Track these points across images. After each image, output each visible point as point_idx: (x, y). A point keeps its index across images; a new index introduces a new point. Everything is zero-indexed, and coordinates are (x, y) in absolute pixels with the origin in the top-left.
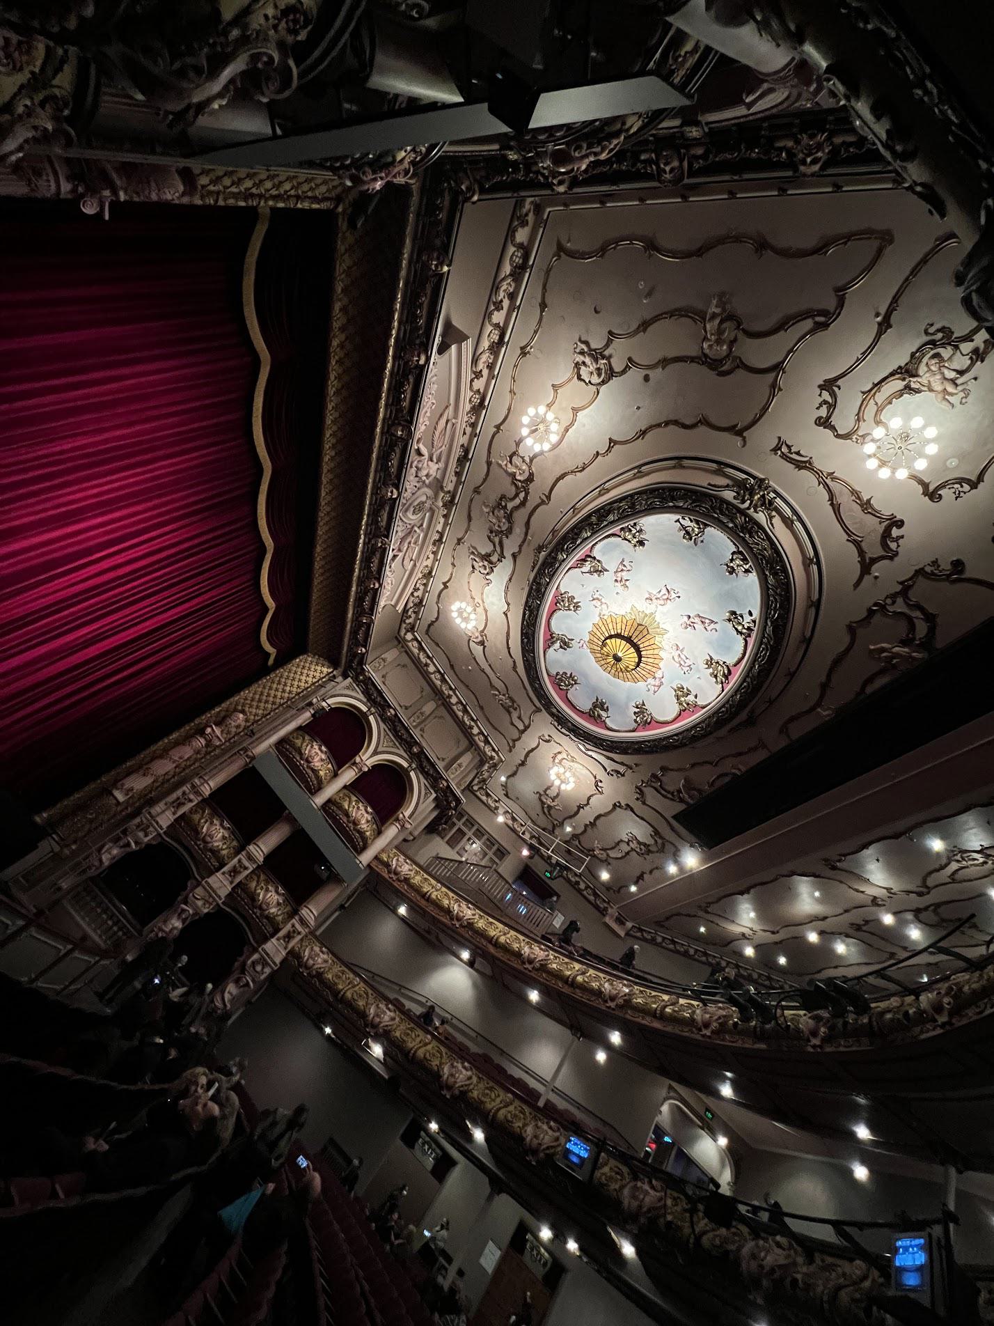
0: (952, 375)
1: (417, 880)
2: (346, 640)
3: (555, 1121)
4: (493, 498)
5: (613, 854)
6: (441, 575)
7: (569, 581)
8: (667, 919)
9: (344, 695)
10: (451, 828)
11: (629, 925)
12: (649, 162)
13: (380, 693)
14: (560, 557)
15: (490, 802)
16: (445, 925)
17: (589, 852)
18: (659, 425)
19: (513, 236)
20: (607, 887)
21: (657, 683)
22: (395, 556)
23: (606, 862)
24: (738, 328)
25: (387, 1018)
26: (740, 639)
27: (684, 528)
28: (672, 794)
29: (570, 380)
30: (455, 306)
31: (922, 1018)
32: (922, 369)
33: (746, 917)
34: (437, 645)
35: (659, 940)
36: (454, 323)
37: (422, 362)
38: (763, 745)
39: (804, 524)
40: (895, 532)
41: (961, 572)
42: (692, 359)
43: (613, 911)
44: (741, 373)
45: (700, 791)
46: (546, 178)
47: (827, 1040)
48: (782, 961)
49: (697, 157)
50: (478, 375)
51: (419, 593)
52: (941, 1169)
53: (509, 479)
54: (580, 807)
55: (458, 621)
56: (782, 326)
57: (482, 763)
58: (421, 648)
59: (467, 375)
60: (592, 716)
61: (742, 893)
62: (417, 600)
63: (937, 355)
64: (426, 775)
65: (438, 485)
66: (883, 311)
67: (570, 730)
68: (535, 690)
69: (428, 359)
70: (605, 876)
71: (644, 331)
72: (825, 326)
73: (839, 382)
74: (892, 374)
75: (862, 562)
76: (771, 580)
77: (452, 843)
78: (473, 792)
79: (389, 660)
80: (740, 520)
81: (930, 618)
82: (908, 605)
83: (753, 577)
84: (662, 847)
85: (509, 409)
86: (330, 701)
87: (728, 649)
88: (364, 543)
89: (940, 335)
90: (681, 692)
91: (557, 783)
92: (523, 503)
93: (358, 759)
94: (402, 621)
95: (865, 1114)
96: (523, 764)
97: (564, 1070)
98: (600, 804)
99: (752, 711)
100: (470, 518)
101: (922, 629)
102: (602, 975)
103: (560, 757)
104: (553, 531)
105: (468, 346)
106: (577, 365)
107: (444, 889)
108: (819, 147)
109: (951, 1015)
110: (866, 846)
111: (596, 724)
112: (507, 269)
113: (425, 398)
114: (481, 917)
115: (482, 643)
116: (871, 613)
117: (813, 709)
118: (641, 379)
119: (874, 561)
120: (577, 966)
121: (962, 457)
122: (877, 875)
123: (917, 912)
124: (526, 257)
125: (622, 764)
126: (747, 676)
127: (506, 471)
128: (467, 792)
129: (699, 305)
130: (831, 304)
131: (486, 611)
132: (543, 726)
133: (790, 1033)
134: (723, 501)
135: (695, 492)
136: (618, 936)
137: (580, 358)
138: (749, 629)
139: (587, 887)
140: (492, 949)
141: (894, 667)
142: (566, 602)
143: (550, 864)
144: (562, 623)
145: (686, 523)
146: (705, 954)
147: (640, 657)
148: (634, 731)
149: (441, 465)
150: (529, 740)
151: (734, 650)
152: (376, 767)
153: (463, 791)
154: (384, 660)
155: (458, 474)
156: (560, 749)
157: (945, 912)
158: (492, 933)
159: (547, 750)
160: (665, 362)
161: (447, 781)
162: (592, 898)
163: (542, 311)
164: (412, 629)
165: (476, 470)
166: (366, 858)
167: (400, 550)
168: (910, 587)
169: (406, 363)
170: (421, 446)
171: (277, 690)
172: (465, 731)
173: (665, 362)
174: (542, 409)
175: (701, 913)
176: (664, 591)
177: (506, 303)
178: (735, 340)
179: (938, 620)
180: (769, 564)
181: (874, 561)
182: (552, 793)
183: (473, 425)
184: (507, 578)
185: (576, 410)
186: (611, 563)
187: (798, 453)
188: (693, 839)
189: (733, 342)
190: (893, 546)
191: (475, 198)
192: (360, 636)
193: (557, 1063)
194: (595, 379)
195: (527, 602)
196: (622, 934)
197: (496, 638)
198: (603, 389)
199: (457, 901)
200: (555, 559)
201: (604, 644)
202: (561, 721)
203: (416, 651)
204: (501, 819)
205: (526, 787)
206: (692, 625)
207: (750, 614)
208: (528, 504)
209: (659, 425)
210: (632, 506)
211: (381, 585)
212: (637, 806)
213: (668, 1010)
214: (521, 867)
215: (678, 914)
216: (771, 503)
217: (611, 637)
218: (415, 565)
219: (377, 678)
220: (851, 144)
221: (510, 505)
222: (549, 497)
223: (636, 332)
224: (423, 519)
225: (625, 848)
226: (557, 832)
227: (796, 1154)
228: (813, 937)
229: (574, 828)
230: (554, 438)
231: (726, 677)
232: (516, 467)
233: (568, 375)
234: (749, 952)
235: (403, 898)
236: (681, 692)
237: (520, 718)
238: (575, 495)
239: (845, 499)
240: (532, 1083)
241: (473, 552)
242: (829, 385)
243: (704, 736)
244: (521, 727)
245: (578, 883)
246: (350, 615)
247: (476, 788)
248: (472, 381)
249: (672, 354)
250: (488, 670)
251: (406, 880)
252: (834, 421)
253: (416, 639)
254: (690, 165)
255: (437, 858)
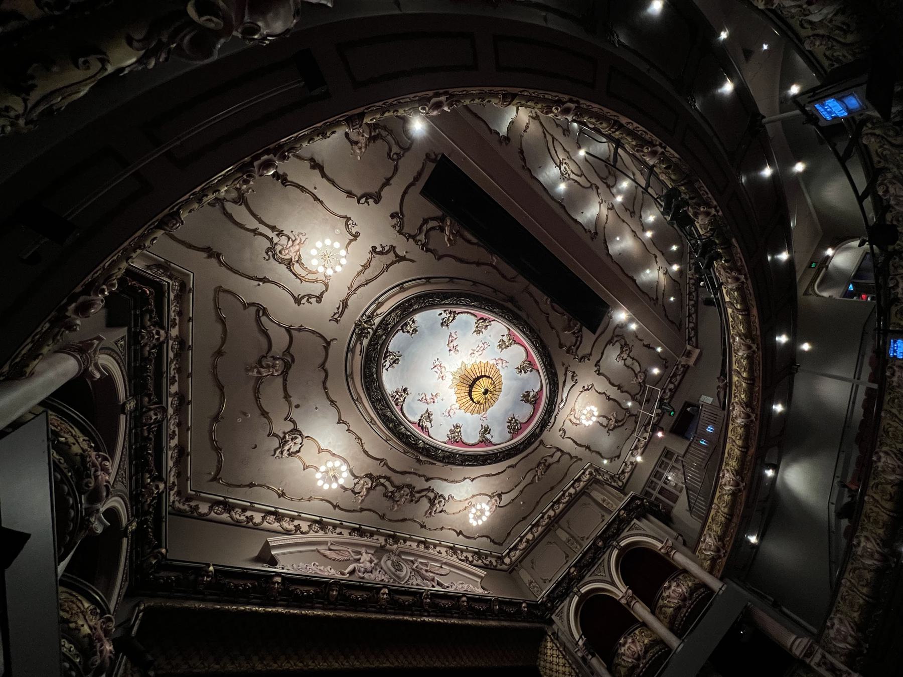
0: (290, 242)
1: (717, 529)
2: (517, 624)
3: (884, 372)
4: (387, 503)
5: (637, 369)
6: (451, 538)
7: (439, 436)
8: (672, 322)
9: (568, 619)
10: (661, 501)
11: (689, 347)
12: (149, 431)
13: (559, 584)
14: (421, 445)
15: (628, 470)
16: (748, 497)
17: (642, 386)
18: (327, 393)
19: (204, 515)
20: (664, 367)
21: (500, 362)
22: (439, 584)
23: (646, 372)
24: (266, 357)
25: (869, 545)
26: (457, 317)
27: (391, 365)
28: (577, 337)
29: (300, 458)
30: (242, 557)
31: (664, 159)
32: (288, 257)
33: (652, 275)
34: (509, 534)
35: (692, 325)
36: (256, 554)
37: (279, 579)
38: (526, 289)
39: (381, 296)
40: (379, 249)
41: (397, 213)
42: (285, 380)
43: (683, 360)
44: (292, 351)
45: (570, 320)
46: (154, 498)
47: (708, 205)
48: (674, 248)
49: (150, 400)
50: (298, 528)
51: (470, 556)
52: (767, 126)
53: (372, 492)
54: (609, 399)
55: (485, 519)
56: (265, 333)
57: (597, 481)
58: (515, 548)
59: (298, 538)
60: (535, 402)
61: (635, 281)
62: (476, 557)
63: (280, 252)
64: (619, 531)
65: (380, 551)
66: (256, 283)
67: (550, 417)
68: (525, 448)
69: (278, 574)
70: (656, 371)
71: (267, 413)
72: (265, 310)
73: (296, 296)
74: (291, 270)
75: (399, 261)
76: (415, 307)
77: (675, 499)
78: (625, 485)
79: (530, 578)
80: (380, 332)
81: (425, 221)
82: (420, 233)
83: (417, 317)
84: (619, 335)
85: (322, 500)
86: (577, 637)
87: (467, 323)
88: (428, 616)
89: (270, 253)
90: (502, 345)
91: (594, 419)
92: (388, 479)
93: (623, 601)
94: (495, 568)
95: (753, 174)
96: (588, 448)
97: (835, 372)
98: (601, 385)
99: (504, 300)
100: (404, 520)
101: (432, 224)
102: (734, 359)
103: (574, 420)
104: (405, 453)
105: (273, 540)
106: (289, 455)
107: (716, 501)
108: (150, 332)
109: (655, 146)
110: (576, 221)
111: (540, 398)
112: (225, 517)
113: (303, 572)
114: (727, 464)
115: (499, 496)
116: (428, 250)
117: (495, 267)
118: (298, 409)
119: (397, 255)
120: (735, 378)
121: (334, 228)
122: (593, 211)
123: (609, 187)
124: (218, 503)
125: (566, 374)
126: (480, 308)
127: (366, 495)
128: (626, 490)
129: (252, 383)
130: (253, 310)
131: (473, 496)
132: (552, 437)
133: (715, 226)
134: (369, 344)
135: (366, 362)
136: (700, 354)
137: (285, 453)
138: (450, 313)
139: (670, 382)
140: (752, 451)
141: (458, 232)
142: (455, 435)
143: (663, 413)
144: (471, 436)
145: (387, 364)
146: (690, 293)
147: (482, 377)
148: (538, 371)
149: (363, 550)
150: (567, 445)
151: (466, 319)
152: (627, 582)
153: (626, 495)
154: (531, 583)
155: (372, 534)
156: (568, 422)
157: (604, 173)
158: (737, 452)
159: (571, 430)
160: (287, 397)
161: (620, 510)
162: (678, 378)
163: (254, 485)
164: (500, 559)
165: (367, 520)
166: (715, 584)
167: (433, 580)
168: (409, 235)
169: (280, 594)
170: (346, 571)
171: (558, 664)
172: (574, 500)
173: (287, 397)
174: (318, 475)
175: (660, 302)
176: (435, 369)
177: (248, 514)
178: (272, 357)
179: (426, 217)
180: (406, 310)
181: (397, 255)
182: (604, 421)
183: (335, 527)
184: (445, 483)
185: (320, 451)
186: (422, 408)
187: (338, 309)
188: (605, 320)
189: (275, 358)
190: (387, 248)
191: (164, 551)
192: (512, 610)
193: (830, 379)
194: (299, 440)
195: (459, 465)
196: (697, 351)
197: (492, 485)
198: (305, 434)
199: (722, 488)
200: (423, 448)
201: (479, 402)
202: (544, 424)
203: (518, 553)
204: (639, 459)
205: (606, 442)
206: (455, 347)
207: (440, 314)
208: (388, 475)
209: (327, 393)
210: (379, 401)
211: (464, 595)
212: (594, 359)
213: (739, 307)
214: (674, 436)
215: (666, 316)
216: (369, 317)
217: (472, 399)
218: (445, 564)
219: (548, 588)
220: (151, 317)
221: (391, 489)
222: (382, 460)
223: (268, 418)
224: (406, 561)
225: (629, 361)
226: (635, 413)
227: (812, 208)
228: (649, 234)
229: (627, 400)
230: (338, 463)
231: (485, 320)
232: (362, 488)
233: (297, 459)
234: (675, 267)
235: (741, 542)
236: (502, 345)
237: (552, 456)
238: (377, 441)
239: (363, 278)
240: (861, 396)
241: (429, 513)
242: (298, 301)
243: (528, 325)
244: (559, 454)
245: (670, 390)
246: (494, 623)
247: (620, 484)
248: (302, 533)
249: (282, 394)
250: (520, 487)
251: (721, 538)
252: (318, 294)
253: (508, 554)
254: (155, 403)
255: (690, 509)
